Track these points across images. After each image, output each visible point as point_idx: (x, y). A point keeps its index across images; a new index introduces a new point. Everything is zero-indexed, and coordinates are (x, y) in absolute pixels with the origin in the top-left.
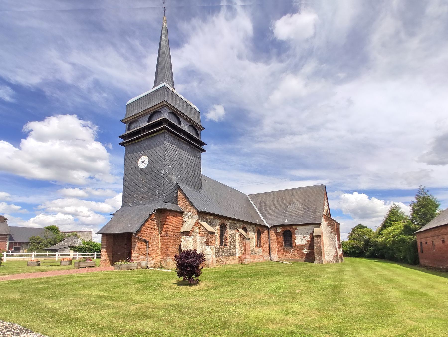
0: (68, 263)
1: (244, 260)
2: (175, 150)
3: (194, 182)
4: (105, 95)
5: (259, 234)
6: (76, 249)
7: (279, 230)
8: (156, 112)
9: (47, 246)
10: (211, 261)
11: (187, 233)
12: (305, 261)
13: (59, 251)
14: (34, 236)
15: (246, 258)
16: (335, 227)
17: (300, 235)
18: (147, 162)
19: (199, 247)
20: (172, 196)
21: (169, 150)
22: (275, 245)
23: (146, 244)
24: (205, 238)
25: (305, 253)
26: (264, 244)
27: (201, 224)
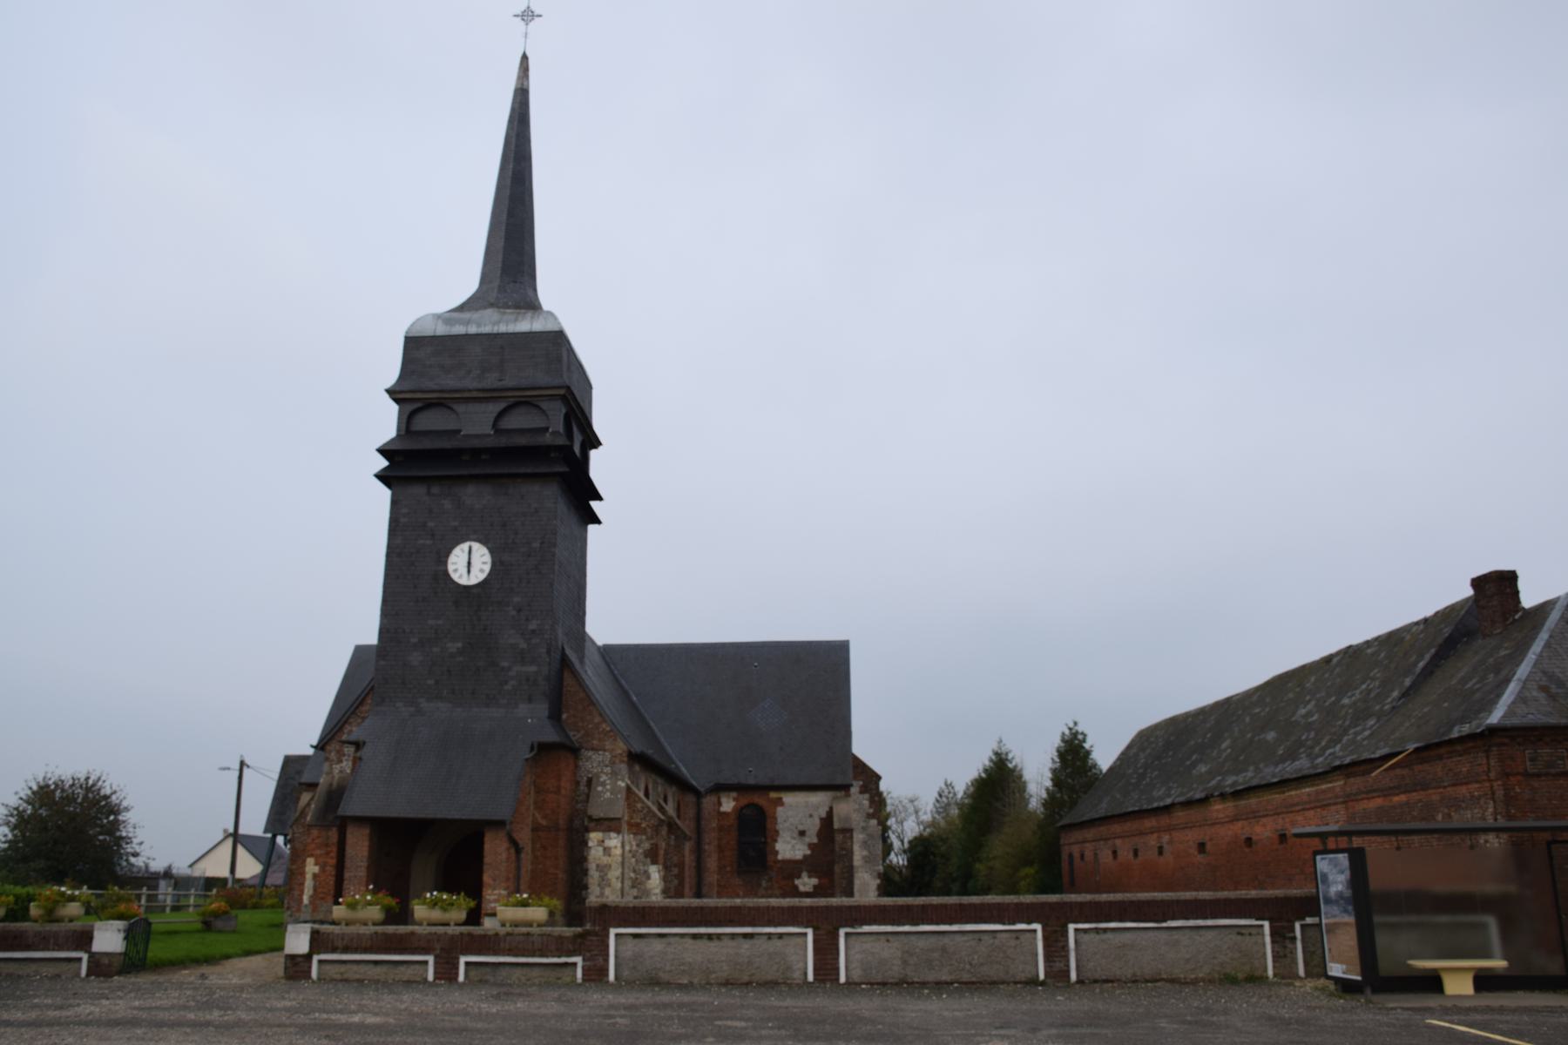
24: (648, 839)
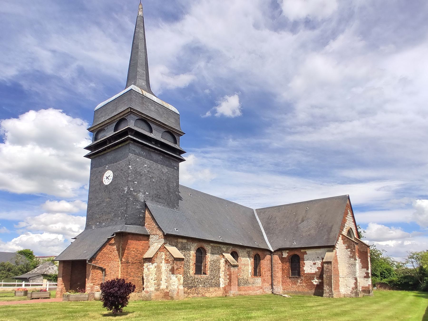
0: (23, 293)
1: (229, 292)
2: (143, 163)
3: (167, 199)
4: (92, 85)
5: (257, 260)
6: (50, 278)
7: (285, 255)
8: (122, 120)
9: (18, 274)
10: (177, 292)
11: (150, 260)
12: (315, 294)
13: (30, 281)
14: (3, 261)
15: (231, 289)
16: (355, 250)
17: (310, 260)
18: (111, 178)
19: (164, 277)
20: (137, 217)
21: (135, 163)
22: (279, 274)
23: (102, 272)
25: (315, 283)
26: (264, 272)
27: (167, 250)
